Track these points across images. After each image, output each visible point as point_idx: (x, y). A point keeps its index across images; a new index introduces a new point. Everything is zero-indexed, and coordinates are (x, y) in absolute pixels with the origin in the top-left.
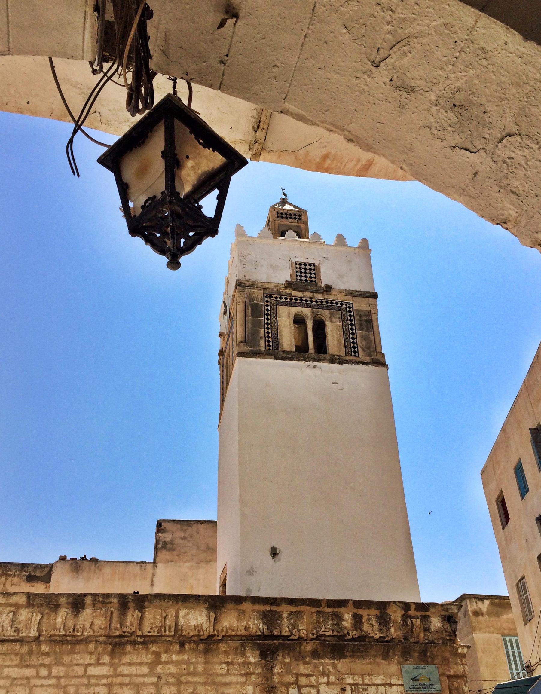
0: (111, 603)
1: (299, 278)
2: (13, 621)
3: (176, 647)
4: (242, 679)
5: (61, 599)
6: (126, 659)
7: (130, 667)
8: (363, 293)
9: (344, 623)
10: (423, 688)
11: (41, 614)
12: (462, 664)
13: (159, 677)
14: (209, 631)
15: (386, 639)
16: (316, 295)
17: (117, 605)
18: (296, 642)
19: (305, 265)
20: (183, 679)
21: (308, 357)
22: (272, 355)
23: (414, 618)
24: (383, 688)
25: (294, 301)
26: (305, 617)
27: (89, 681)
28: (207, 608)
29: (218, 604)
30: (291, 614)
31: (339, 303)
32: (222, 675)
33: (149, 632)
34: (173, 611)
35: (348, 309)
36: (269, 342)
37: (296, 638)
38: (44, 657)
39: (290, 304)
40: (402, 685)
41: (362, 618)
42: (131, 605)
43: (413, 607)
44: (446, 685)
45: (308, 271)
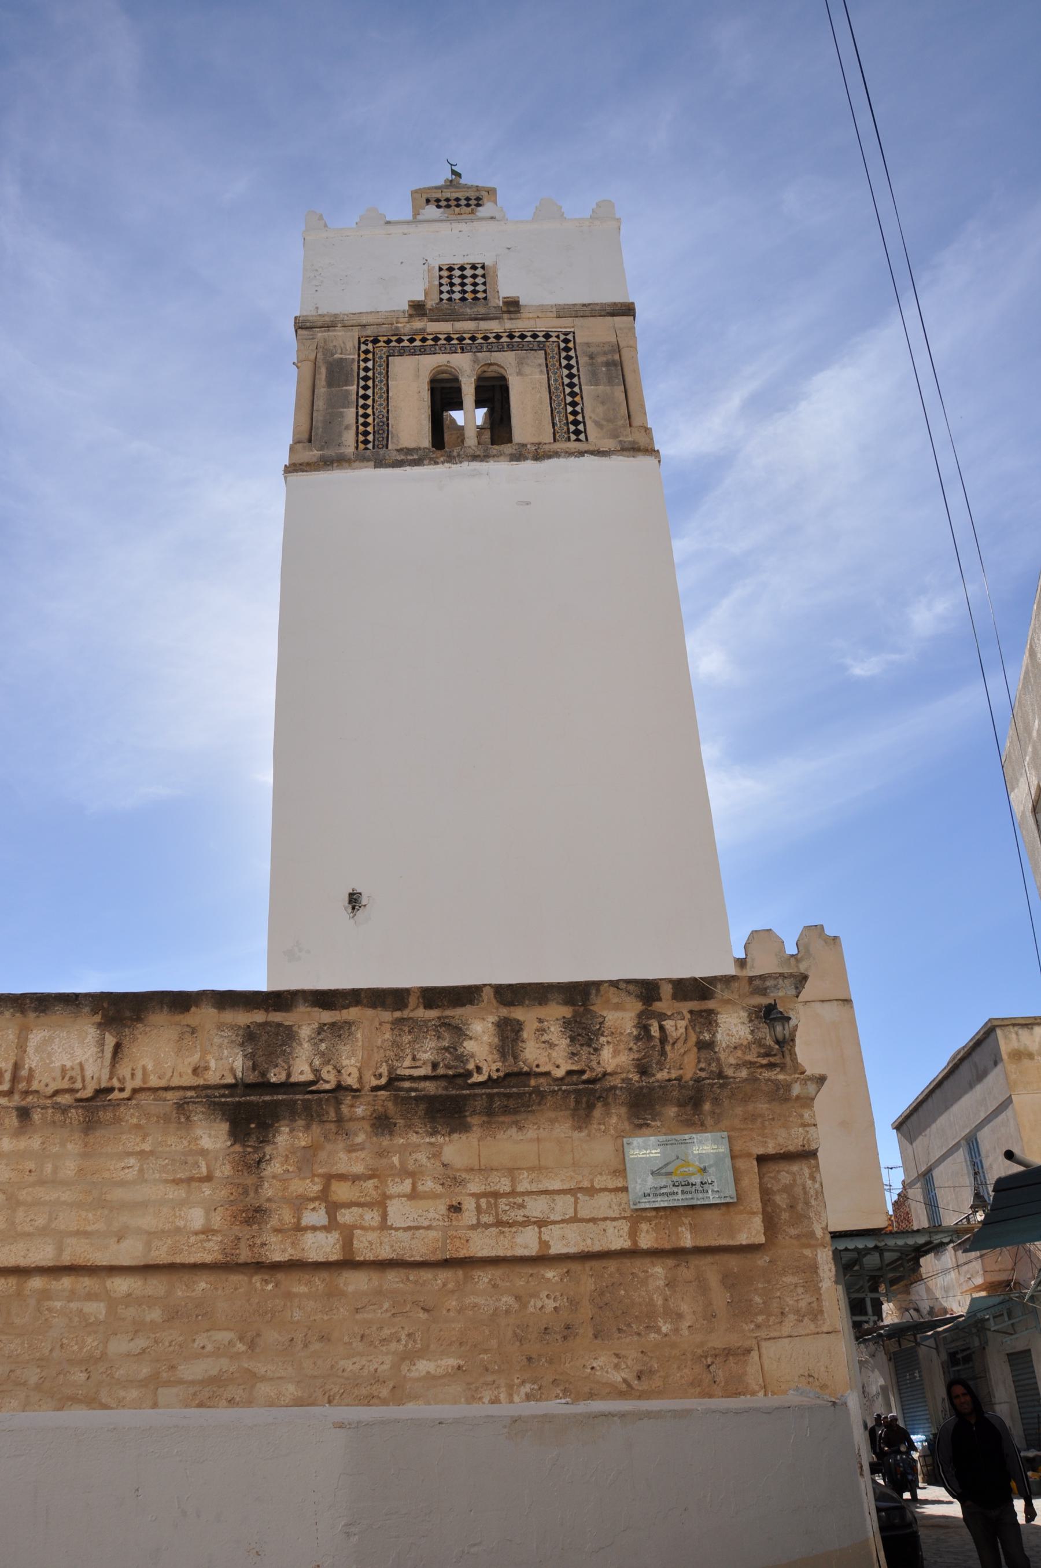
1: (445, 296)
4: (180, 1193)
8: (598, 308)
9: (469, 1046)
10: (683, 1192)
12: (804, 1125)
15: (585, 1077)
16: (484, 325)
18: (326, 1096)
19: (462, 268)
20: (23, 1195)
21: (459, 455)
22: (369, 460)
23: (669, 1017)
25: (430, 342)
26: (359, 1035)
30: (320, 1030)
32: (123, 1183)
35: (562, 345)
37: (327, 1087)
39: (422, 351)
41: (521, 1029)
43: (667, 990)
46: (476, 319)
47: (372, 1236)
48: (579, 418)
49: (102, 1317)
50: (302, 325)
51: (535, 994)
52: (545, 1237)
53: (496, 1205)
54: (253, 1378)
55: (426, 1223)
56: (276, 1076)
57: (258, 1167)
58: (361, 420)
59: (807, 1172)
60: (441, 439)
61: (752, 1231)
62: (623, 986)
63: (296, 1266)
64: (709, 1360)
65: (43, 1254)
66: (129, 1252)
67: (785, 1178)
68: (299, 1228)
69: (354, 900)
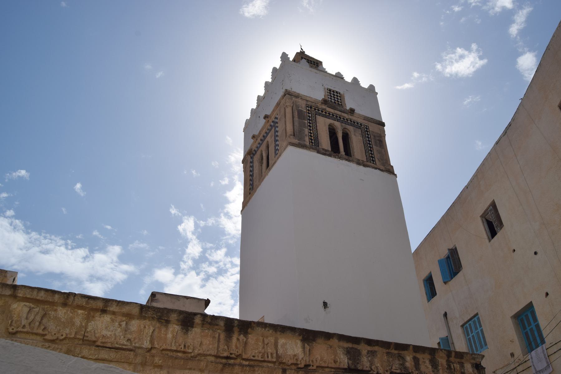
0: (217, 325)
2: (126, 330)
5: (173, 315)
11: (153, 327)
14: (306, 361)
17: (224, 328)
28: (302, 340)
29: (311, 338)
30: (368, 352)
33: (254, 356)
34: (272, 340)
38: (156, 369)
43: (453, 354)
69: (325, 305)
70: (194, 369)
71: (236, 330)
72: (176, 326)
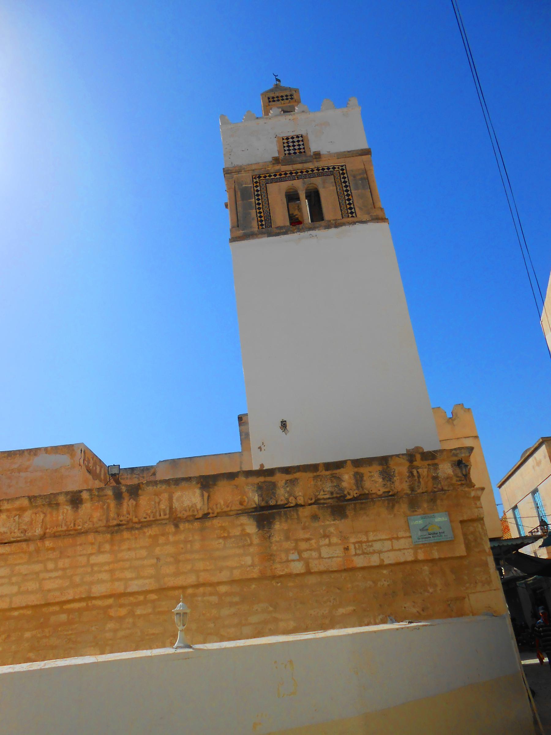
1: (287, 152)
3: (172, 529)
4: (241, 551)
6: (125, 546)
7: (129, 552)
12: (477, 508)
13: (158, 559)
15: (390, 494)
19: (293, 138)
21: (303, 228)
23: (420, 468)
24: (389, 542)
27: (92, 570)
28: (200, 488)
29: (211, 483)
31: (331, 167)
35: (341, 172)
36: (261, 221)
37: (292, 505)
38: (50, 552)
39: (281, 180)
40: (410, 537)
42: (126, 495)
43: (418, 457)
44: (459, 532)
45: (296, 144)
46: (302, 163)
47: (316, 562)
48: (352, 206)
49: (217, 602)
50: (227, 172)
51: (369, 461)
52: (382, 558)
53: (362, 546)
54: (276, 620)
55: (336, 555)
56: (272, 503)
57: (269, 539)
58: (259, 215)
59: (480, 526)
60: (295, 223)
61: (461, 551)
62: (401, 456)
63: (290, 576)
64: (449, 602)
65: (192, 579)
66: (224, 576)
67: (471, 529)
68: (288, 561)
69: (284, 425)
70: (85, 544)
71: (126, 495)
72: (67, 507)
